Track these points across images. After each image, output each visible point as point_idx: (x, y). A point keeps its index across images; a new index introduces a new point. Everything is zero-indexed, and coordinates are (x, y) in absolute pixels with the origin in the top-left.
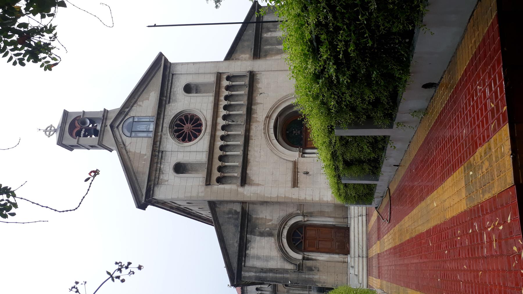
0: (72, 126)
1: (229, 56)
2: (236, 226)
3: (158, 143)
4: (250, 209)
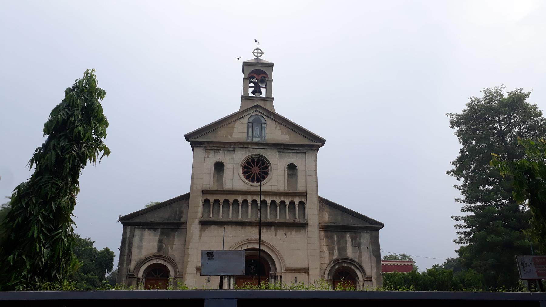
1: (323, 202)
3: (242, 146)
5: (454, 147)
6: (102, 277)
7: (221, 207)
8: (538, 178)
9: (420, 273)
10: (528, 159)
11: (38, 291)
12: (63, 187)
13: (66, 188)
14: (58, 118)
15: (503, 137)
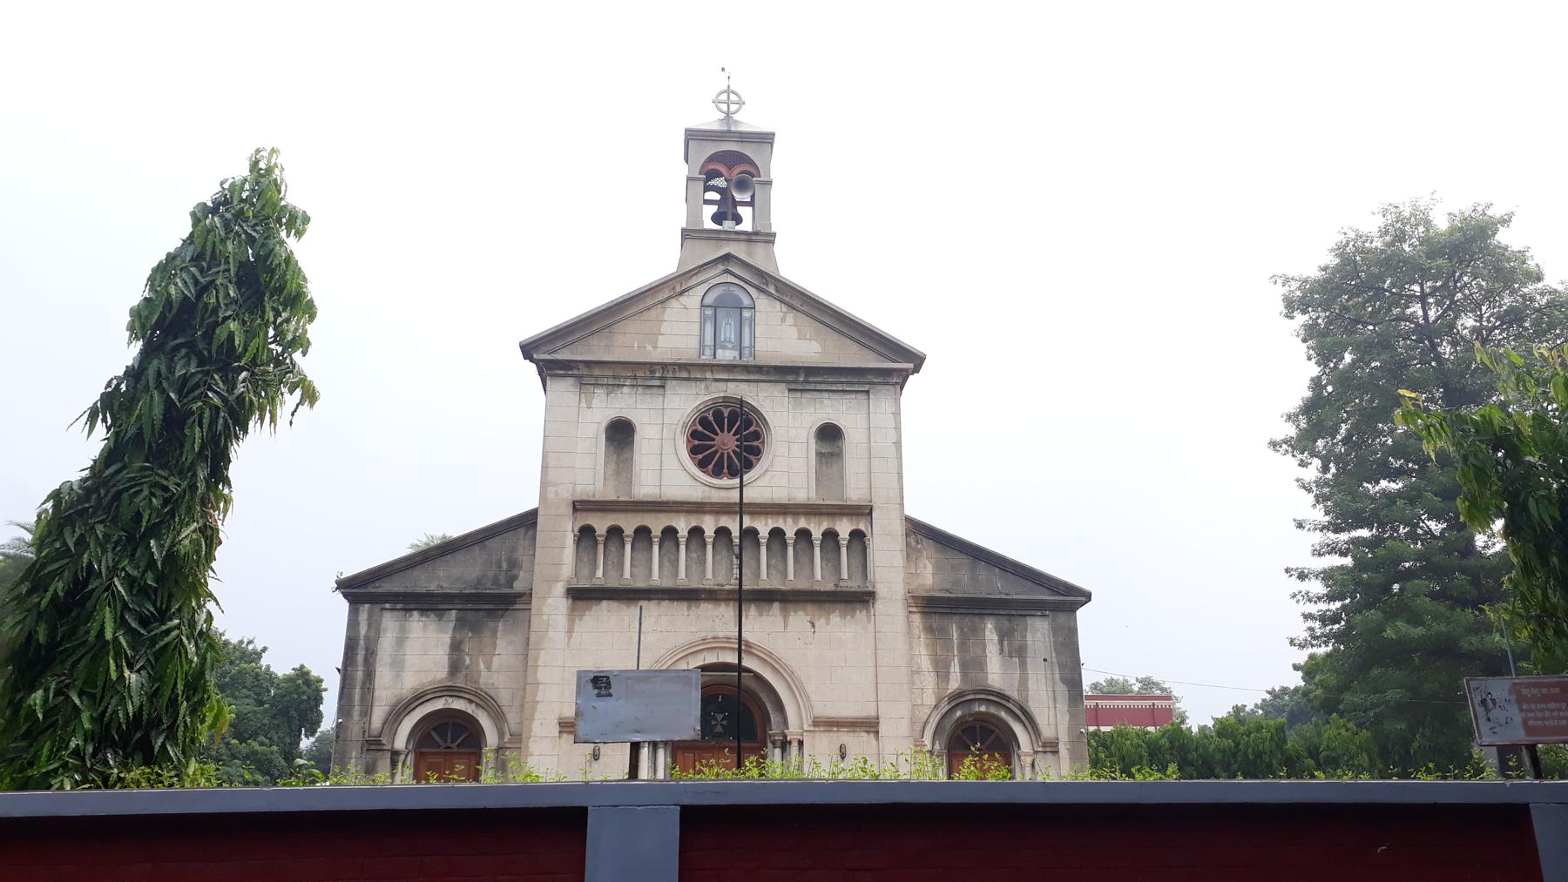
0: (732, 159)
1: (919, 531)
2: (479, 582)
3: (685, 375)
4: (519, 614)
5: (1290, 372)
6: (290, 753)
7: (628, 547)
8: (1529, 458)
9: (1195, 730)
10: (1503, 406)
11: (117, 790)
12: (182, 496)
13: (192, 498)
14: (169, 295)
15: (1431, 342)
